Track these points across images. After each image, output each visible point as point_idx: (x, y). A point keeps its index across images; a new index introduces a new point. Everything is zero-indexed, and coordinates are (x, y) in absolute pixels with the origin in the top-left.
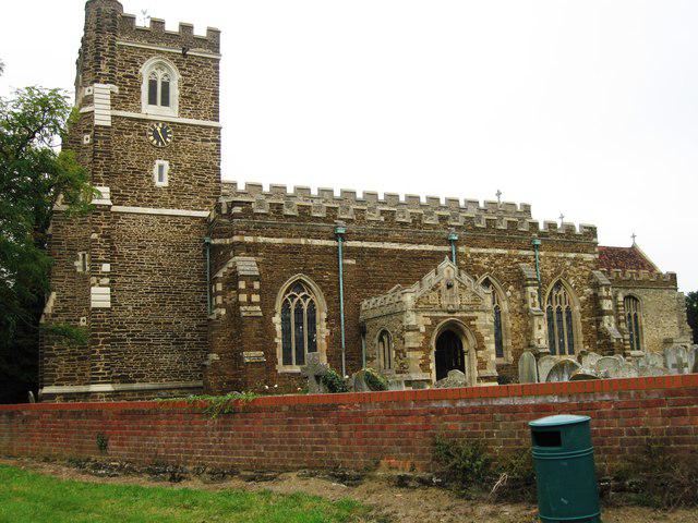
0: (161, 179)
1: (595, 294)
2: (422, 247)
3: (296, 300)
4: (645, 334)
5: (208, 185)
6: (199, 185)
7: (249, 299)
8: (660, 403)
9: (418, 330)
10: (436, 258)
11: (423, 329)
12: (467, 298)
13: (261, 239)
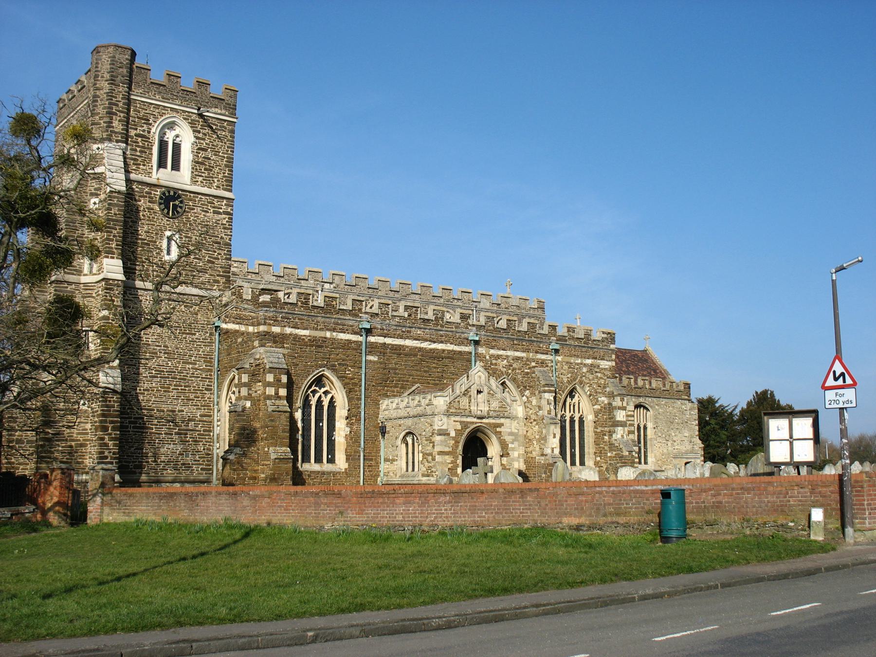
0: (169, 253)
1: (610, 404)
2: (440, 346)
3: (317, 396)
4: (396, 400)
5: (216, 261)
6: (209, 262)
7: (277, 393)
8: (710, 490)
9: (449, 434)
10: (463, 363)
11: (453, 434)
12: (495, 405)
13: (288, 330)
